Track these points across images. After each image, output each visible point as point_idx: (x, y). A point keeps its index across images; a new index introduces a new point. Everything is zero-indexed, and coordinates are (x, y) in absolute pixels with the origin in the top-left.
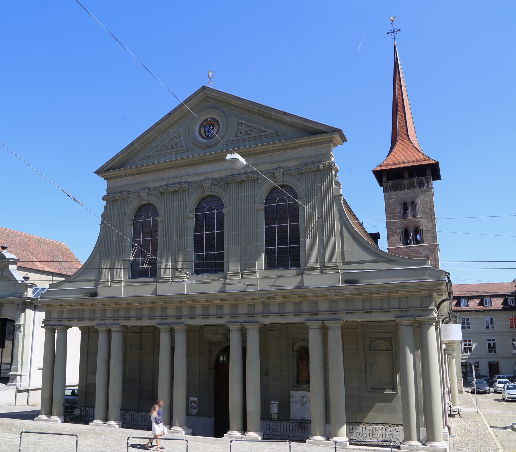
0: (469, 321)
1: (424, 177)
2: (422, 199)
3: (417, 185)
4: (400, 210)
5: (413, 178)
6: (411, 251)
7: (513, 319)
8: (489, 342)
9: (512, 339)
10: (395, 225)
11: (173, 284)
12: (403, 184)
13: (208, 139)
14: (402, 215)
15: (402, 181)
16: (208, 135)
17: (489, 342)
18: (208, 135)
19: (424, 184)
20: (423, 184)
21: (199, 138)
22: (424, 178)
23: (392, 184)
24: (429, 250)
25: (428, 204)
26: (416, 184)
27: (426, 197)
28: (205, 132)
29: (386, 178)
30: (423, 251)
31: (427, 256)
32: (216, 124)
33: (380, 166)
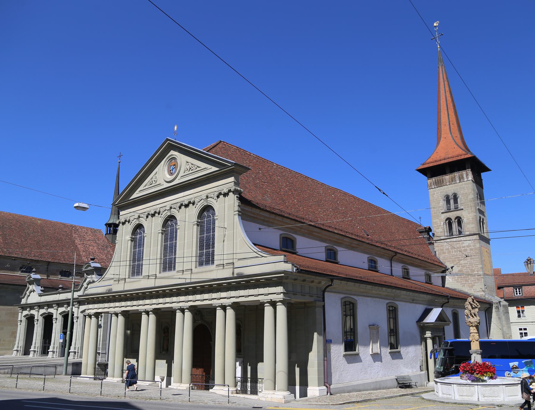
3: (458, 179)
4: (443, 204)
8: (521, 331)
9: (519, 329)
10: (439, 219)
11: (119, 284)
12: (445, 179)
13: (172, 176)
14: (445, 208)
15: (444, 177)
16: (172, 172)
17: (521, 331)
19: (464, 178)
20: (463, 177)
23: (435, 180)
25: (468, 197)
26: (457, 178)
27: (466, 190)
31: (469, 245)
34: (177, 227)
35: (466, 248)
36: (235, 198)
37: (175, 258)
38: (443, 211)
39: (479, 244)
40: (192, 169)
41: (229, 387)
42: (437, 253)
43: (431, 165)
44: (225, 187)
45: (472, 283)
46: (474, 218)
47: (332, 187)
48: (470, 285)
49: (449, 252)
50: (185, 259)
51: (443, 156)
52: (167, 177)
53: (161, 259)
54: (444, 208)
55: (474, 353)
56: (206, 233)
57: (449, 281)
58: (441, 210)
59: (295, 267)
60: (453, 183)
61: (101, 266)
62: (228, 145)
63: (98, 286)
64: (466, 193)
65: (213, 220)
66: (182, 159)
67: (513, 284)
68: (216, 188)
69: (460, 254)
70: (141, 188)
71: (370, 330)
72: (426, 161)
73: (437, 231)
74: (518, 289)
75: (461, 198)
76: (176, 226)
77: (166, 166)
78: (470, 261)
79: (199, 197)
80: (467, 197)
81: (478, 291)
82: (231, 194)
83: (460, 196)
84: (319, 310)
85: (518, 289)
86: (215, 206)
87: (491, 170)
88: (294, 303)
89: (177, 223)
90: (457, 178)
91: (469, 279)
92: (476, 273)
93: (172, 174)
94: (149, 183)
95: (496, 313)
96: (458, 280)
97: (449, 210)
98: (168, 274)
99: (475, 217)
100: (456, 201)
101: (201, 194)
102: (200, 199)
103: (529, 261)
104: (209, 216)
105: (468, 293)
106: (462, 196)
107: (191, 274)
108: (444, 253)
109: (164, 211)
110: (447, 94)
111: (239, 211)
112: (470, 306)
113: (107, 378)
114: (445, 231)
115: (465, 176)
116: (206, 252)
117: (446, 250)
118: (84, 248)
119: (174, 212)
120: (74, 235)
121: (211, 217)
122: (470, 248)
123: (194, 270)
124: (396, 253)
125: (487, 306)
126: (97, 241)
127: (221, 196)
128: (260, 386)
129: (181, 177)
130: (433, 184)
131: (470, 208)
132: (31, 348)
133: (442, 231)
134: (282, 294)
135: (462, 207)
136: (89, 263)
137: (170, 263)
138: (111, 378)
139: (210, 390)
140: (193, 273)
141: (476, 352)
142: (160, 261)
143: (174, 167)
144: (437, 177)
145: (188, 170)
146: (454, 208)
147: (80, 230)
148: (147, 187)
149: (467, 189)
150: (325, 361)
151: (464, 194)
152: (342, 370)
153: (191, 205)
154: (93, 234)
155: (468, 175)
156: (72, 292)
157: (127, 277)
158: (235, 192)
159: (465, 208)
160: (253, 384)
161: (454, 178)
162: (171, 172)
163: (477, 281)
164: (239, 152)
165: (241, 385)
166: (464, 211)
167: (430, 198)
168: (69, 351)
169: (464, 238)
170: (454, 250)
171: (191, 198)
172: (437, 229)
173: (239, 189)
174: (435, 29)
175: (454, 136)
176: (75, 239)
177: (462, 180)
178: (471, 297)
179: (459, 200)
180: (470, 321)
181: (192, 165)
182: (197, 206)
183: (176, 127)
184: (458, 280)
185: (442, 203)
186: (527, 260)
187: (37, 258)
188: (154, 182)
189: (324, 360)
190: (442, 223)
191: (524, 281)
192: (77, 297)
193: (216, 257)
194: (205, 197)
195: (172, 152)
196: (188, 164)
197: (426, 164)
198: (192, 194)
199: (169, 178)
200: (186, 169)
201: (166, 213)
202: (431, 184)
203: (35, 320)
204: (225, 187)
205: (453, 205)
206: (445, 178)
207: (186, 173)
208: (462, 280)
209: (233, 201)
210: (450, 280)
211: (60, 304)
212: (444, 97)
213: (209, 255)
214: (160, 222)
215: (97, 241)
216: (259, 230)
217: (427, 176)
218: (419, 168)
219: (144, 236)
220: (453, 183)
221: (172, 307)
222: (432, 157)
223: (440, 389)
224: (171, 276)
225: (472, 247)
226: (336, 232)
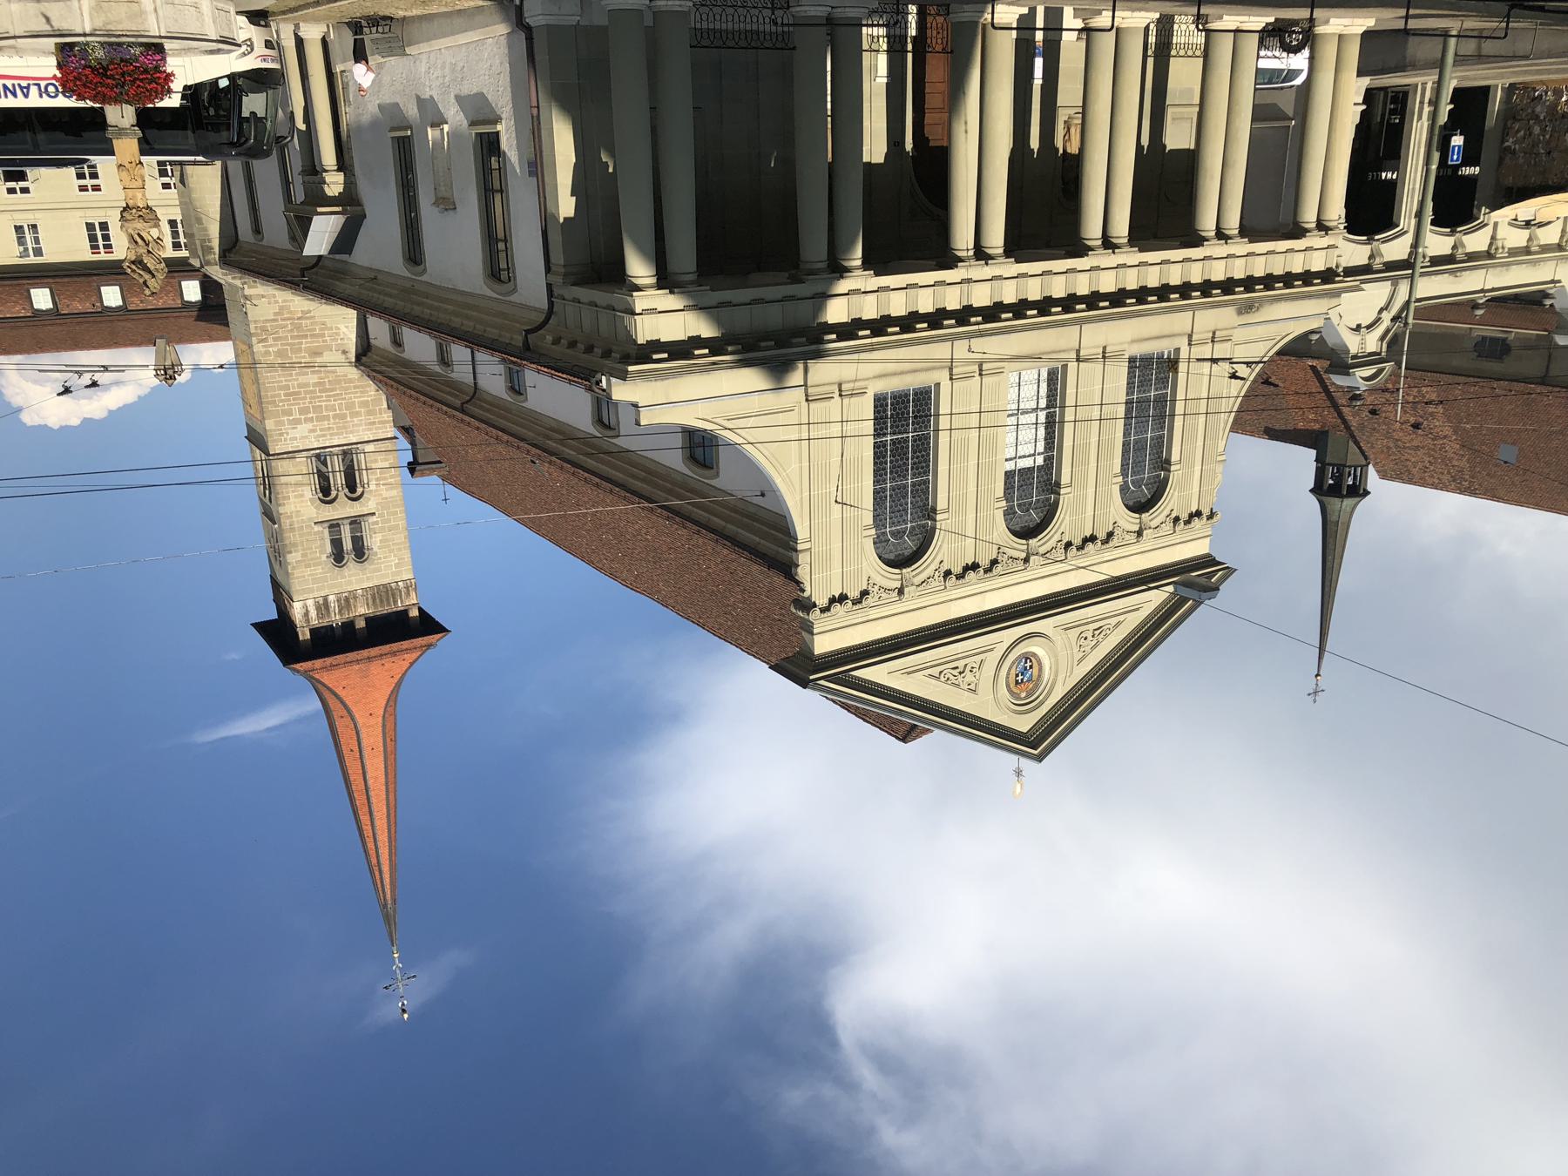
0: (110, 241)
1: (317, 626)
2: (318, 569)
3: (332, 605)
4: (371, 537)
5: (344, 620)
6: (337, 434)
7: (101, 247)
9: (29, 192)
11: (1213, 329)
12: (368, 604)
13: (1026, 653)
16: (1026, 662)
17: (95, 182)
18: (1026, 662)
20: (318, 608)
21: (1044, 653)
22: (315, 622)
23: (395, 602)
24: (291, 439)
25: (302, 557)
26: (335, 607)
27: (309, 575)
28: (1031, 667)
29: (411, 615)
30: (306, 437)
32: (1012, 685)
33: (429, 646)
34: (1004, 503)
35: (303, 417)
36: (808, 588)
38: (374, 519)
39: (267, 428)
40: (955, 672)
42: (385, 406)
43: (405, 644)
44: (840, 620)
45: (283, 320)
46: (284, 498)
48: (288, 316)
49: (350, 406)
50: (836, 429)
51: (375, 668)
52: (1041, 649)
53: (937, 430)
55: (126, 129)
57: (347, 327)
58: (377, 523)
59: (604, 390)
60: (346, 594)
61: (1331, 375)
63: (1292, 323)
64: (308, 566)
66: (992, 704)
68: (871, 617)
69: (319, 402)
71: (453, 195)
72: (421, 655)
75: (321, 553)
76: (1012, 507)
77: (1046, 679)
78: (290, 381)
79: (929, 591)
80: (303, 555)
81: (263, 296)
82: (822, 601)
83: (324, 557)
84: (558, 258)
86: (877, 567)
87: (256, 625)
89: (874, 543)
90: (335, 607)
91: (292, 330)
92: (271, 349)
93: (1026, 659)
94: (1104, 633)
95: (208, 235)
96: (321, 329)
97: (356, 522)
99: (281, 502)
100: (337, 544)
102: (924, 584)
103: (171, 377)
105: (292, 293)
106: (320, 558)
107: (1192, 332)
108: (365, 404)
109: (1051, 550)
110: (371, 831)
111: (796, 551)
112: (152, 268)
115: (313, 613)
117: (358, 414)
119: (1129, 521)
120: (1464, 463)
121: (1019, 505)
122: (291, 418)
123: (1183, 343)
124: (463, 411)
125: (232, 257)
126: (1391, 445)
127: (854, 593)
129: (992, 650)
130: (400, 591)
131: (296, 526)
134: (638, 310)
135: (317, 528)
140: (1185, 334)
141: (121, 132)
142: (937, 423)
143: (1020, 677)
144: (389, 611)
145: (968, 668)
146: (342, 527)
148: (1114, 621)
149: (304, 577)
150: (535, 104)
152: (502, 75)
153: (958, 569)
155: (304, 613)
157: (1072, 366)
158: (808, 606)
159: (310, 526)
161: (342, 609)
163: (268, 324)
165: (906, 28)
167: (409, 555)
170: (336, 410)
171: (956, 590)
173: (801, 614)
174: (405, 1002)
175: (347, 720)
176: (1461, 452)
177: (321, 602)
178: (153, 293)
179: (329, 549)
180: (145, 224)
181: (957, 682)
182: (1057, 537)
184: (321, 329)
185: (373, 541)
186: (175, 379)
188: (1089, 635)
189: (538, 107)
190: (373, 487)
192: (1363, 286)
193: (870, 413)
194: (906, 590)
195: (1024, 724)
196: (969, 687)
197: (421, 647)
198: (951, 600)
200: (974, 670)
201: (916, 575)
202: (408, 594)
204: (840, 620)
205: (364, 533)
206: (369, 610)
207: (978, 658)
208: (309, 330)
209: (818, 580)
210: (345, 330)
212: (377, 823)
213: (915, 417)
214: (1172, 495)
215: (1391, 445)
220: (346, 594)
221: (1141, 251)
222: (406, 664)
223: (206, 19)
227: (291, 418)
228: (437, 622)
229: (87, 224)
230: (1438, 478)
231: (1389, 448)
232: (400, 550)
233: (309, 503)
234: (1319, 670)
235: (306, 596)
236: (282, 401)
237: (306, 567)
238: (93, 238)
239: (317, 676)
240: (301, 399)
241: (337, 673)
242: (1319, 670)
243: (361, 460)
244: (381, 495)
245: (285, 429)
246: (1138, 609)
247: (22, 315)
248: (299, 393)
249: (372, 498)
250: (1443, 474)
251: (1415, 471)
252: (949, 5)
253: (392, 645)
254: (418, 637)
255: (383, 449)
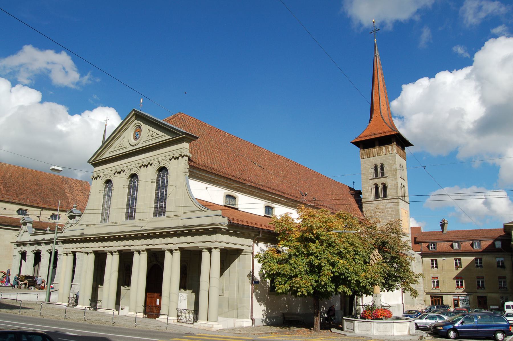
25: (392, 167)
27: (391, 161)
33: (357, 138)
37: (135, 209)
38: (371, 178)
41: (113, 311)
43: (363, 139)
47: (277, 155)
54: (372, 176)
56: (161, 190)
58: (370, 176)
62: (187, 116)
63: (74, 229)
65: (167, 179)
67: (429, 240)
70: (111, 149)
73: (366, 194)
74: (433, 245)
80: (392, 167)
85: (433, 245)
87: (413, 145)
88: (229, 250)
93: (136, 139)
98: (130, 222)
101: (151, 159)
104: (164, 176)
106: (387, 166)
113: (78, 306)
114: (372, 195)
116: (160, 205)
118: (72, 197)
120: (65, 186)
122: (392, 209)
126: (84, 191)
128: (185, 315)
129: (143, 142)
132: (54, 281)
133: (369, 194)
136: (72, 210)
137: (132, 212)
138: (357, 325)
139: (157, 319)
143: (138, 133)
147: (70, 182)
148: (116, 149)
151: (389, 164)
154: (80, 185)
156: (56, 233)
160: (196, 315)
162: (136, 137)
164: (196, 122)
166: (388, 179)
168: (72, 284)
169: (387, 201)
172: (365, 192)
176: (65, 189)
181: (153, 133)
183: (142, 100)
187: (32, 203)
191: (438, 238)
198: (152, 156)
199: (133, 142)
203: (27, 256)
211: (47, 243)
215: (84, 191)
216: (205, 189)
217: (359, 147)
218: (353, 141)
219: (112, 190)
224: (105, 227)
225: (393, 209)
226: (274, 192)
227: (392, 209)
228: (355, 145)
229: (437, 268)
230: (72, 182)
231: (85, 191)
232: (364, 168)
233: (389, 183)
234: (106, 127)
235: (392, 154)
236: (393, 214)
237: (391, 163)
238: (436, 264)
239: (391, 129)
240: (388, 215)
241: (385, 130)
242: (106, 127)
243: (374, 196)
244: (368, 185)
245: (393, 206)
246: (111, 152)
247: (484, 241)
248: (389, 216)
249: (370, 184)
250: (71, 183)
251: (78, 184)
252: (143, 317)
253: (383, 135)
254: (360, 141)
255: (366, 199)
